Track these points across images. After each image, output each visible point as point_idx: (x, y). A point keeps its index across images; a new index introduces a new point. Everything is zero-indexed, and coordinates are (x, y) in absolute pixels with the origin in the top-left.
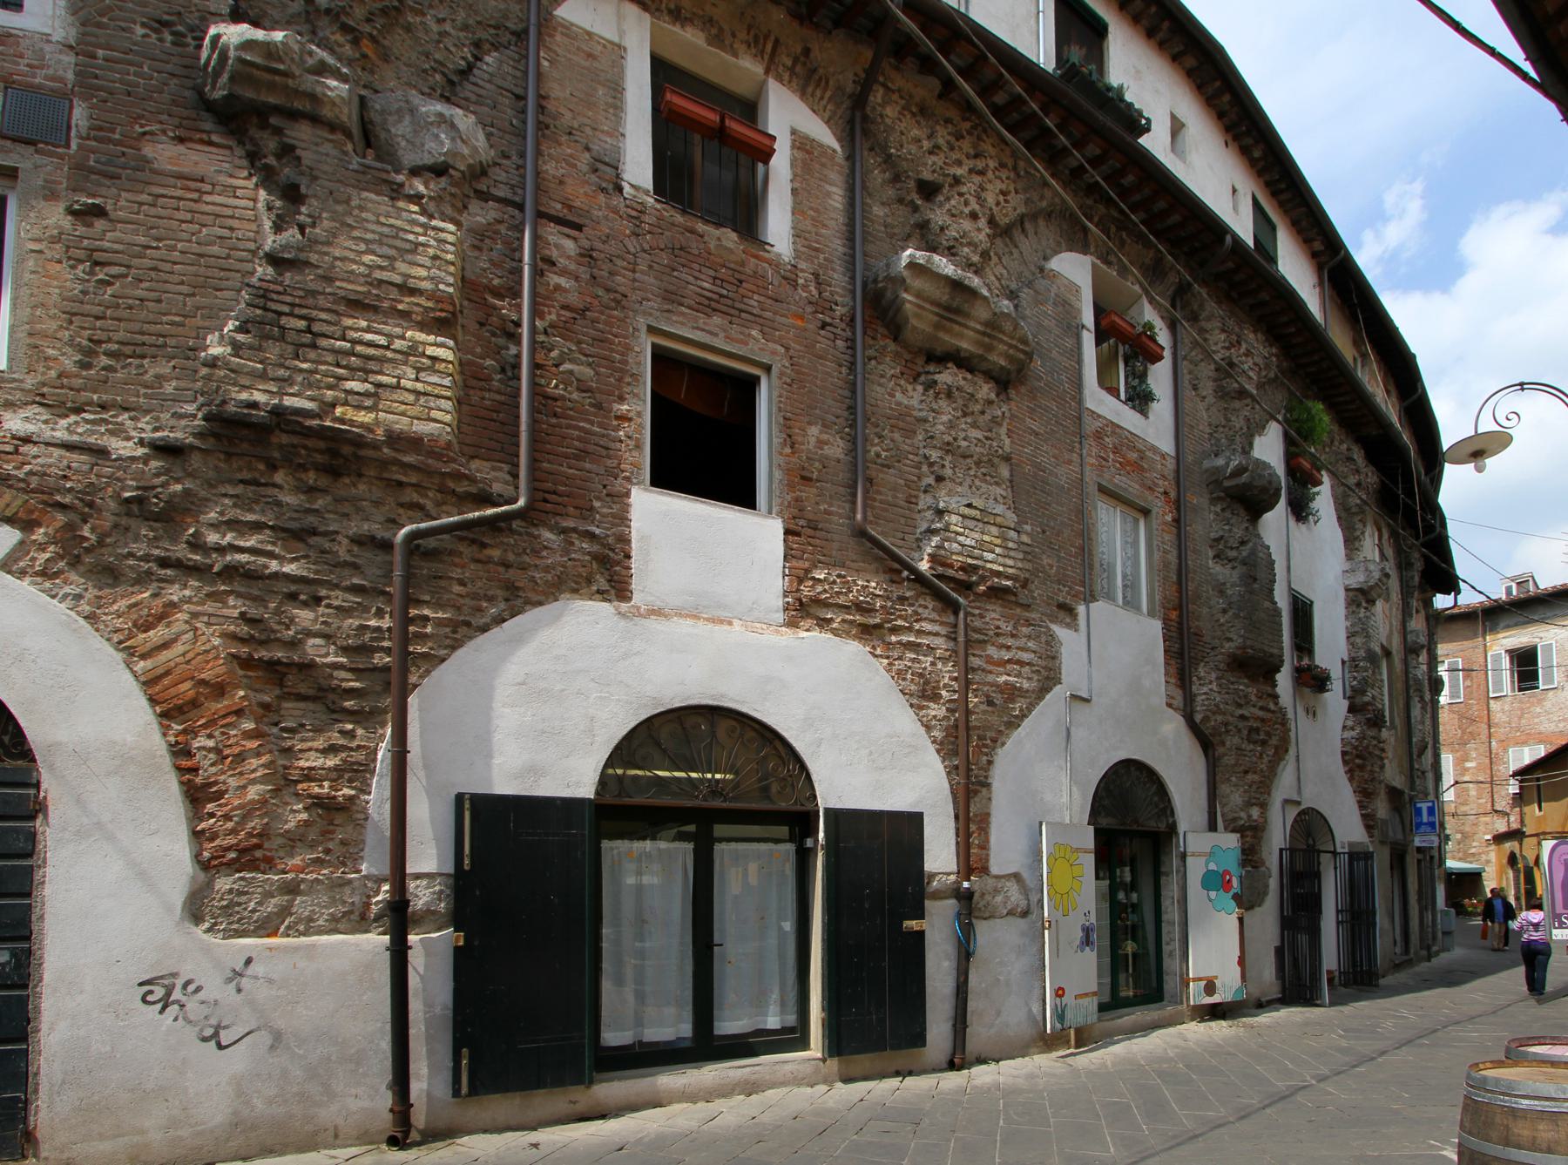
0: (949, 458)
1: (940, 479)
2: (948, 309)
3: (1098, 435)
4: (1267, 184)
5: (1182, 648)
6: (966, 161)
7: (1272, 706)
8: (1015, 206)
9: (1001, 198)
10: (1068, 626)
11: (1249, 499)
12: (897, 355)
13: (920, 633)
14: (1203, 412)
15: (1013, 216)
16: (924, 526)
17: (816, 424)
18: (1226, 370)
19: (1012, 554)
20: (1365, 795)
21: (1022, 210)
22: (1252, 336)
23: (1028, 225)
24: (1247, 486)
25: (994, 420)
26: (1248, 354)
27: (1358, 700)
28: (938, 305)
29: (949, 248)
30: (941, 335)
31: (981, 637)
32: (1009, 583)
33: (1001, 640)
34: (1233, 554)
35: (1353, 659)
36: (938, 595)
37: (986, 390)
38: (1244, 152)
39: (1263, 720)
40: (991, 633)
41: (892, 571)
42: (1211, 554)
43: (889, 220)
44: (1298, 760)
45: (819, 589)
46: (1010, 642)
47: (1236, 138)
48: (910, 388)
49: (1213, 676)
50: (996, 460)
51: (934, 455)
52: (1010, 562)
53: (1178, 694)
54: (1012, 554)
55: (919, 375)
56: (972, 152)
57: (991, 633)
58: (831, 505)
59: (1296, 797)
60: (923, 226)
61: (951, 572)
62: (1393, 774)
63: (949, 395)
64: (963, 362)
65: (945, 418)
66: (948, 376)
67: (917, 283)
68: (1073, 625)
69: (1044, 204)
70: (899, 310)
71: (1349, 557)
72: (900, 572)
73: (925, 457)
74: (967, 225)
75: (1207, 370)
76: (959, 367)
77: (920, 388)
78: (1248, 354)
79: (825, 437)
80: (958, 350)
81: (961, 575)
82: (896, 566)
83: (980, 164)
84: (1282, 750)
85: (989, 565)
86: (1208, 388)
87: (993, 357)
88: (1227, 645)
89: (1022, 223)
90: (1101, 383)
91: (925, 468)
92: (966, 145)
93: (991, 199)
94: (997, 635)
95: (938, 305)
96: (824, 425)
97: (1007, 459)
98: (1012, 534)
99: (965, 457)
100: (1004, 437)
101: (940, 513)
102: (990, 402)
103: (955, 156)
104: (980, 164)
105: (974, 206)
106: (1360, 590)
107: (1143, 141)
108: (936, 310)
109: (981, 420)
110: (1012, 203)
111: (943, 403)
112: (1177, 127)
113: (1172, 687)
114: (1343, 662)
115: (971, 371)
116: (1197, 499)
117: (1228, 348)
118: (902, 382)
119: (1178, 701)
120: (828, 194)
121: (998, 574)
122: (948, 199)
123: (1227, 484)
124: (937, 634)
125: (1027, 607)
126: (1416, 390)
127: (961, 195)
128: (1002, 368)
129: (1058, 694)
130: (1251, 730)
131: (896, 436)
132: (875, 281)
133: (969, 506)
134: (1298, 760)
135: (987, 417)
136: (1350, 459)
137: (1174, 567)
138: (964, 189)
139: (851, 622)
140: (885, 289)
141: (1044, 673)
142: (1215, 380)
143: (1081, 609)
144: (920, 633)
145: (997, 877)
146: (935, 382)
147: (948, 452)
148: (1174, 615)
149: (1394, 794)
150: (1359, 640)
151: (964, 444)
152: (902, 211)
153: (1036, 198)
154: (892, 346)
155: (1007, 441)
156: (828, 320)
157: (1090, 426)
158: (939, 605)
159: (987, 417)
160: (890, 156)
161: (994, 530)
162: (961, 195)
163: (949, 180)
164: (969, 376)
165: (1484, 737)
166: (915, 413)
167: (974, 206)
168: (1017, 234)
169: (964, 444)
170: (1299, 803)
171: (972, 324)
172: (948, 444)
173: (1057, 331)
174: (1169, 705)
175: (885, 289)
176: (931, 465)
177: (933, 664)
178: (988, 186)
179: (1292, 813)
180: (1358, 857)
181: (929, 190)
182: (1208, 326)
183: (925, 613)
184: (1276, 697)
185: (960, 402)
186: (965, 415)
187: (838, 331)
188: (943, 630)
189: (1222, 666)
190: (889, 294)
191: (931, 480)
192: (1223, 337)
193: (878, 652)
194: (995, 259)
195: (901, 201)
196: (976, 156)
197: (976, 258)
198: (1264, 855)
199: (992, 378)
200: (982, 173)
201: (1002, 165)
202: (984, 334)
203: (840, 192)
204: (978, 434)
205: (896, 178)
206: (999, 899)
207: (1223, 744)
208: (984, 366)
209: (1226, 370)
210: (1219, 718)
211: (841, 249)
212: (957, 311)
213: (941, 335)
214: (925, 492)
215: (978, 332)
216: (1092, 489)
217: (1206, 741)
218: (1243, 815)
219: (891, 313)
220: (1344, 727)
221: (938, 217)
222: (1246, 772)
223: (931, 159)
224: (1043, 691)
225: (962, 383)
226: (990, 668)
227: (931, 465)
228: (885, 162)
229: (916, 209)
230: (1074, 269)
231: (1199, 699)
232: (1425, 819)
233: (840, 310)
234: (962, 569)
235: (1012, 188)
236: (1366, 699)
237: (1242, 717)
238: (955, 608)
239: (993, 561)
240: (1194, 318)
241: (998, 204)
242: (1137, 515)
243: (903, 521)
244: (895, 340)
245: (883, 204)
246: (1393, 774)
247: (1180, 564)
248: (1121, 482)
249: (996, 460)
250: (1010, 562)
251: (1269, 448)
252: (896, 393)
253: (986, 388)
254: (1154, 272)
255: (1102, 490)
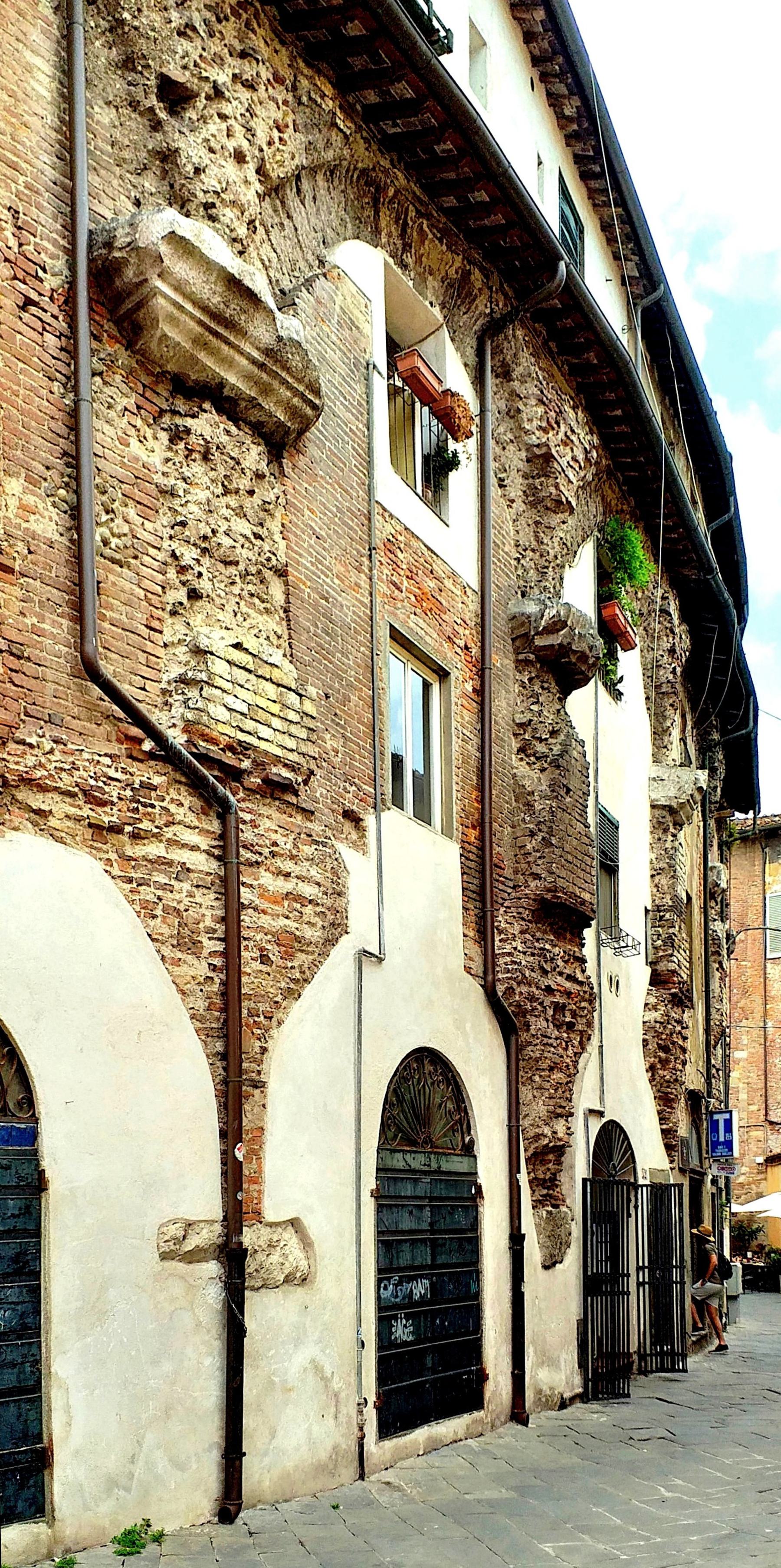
0: (206, 561)
1: (194, 595)
2: (216, 316)
3: (391, 545)
4: (578, 159)
5: (482, 886)
6: (229, 60)
7: (580, 976)
8: (290, 155)
9: (276, 134)
10: (354, 845)
11: (561, 666)
12: (130, 373)
13: (172, 843)
14: (510, 522)
15: (290, 166)
16: (175, 671)
17: (17, 475)
18: (541, 462)
19: (294, 729)
20: (665, 1100)
21: (302, 159)
22: (571, 414)
23: (306, 185)
24: (564, 649)
25: (265, 506)
26: (567, 442)
27: (662, 967)
28: (205, 309)
29: (208, 206)
30: (202, 356)
31: (254, 858)
32: (286, 773)
33: (279, 862)
34: (541, 748)
35: (658, 908)
36: (197, 785)
37: (254, 456)
38: (554, 101)
39: (568, 994)
40: (266, 851)
41: (129, 739)
42: (515, 745)
43: (117, 134)
44: (601, 1053)
45: (31, 761)
46: (287, 866)
47: (544, 77)
48: (149, 433)
49: (516, 929)
50: (268, 574)
51: (189, 555)
52: (291, 743)
53: (475, 951)
54: (294, 729)
55: (162, 412)
56: (239, 47)
57: (266, 851)
58: (42, 620)
59: (597, 1107)
60: (167, 157)
61: (214, 751)
62: (693, 1079)
63: (206, 457)
64: (229, 406)
65: (202, 495)
66: (207, 425)
67: (181, 268)
68: (360, 845)
69: (330, 155)
70: (141, 304)
71: (656, 761)
72: (140, 741)
73: (174, 555)
74: (231, 169)
75: (516, 458)
76: (220, 411)
77: (164, 436)
78: (567, 442)
79: (30, 500)
80: (222, 384)
81: (229, 758)
82: (135, 731)
83: (249, 70)
84: (585, 1039)
85: (263, 745)
86: (516, 486)
87: (268, 404)
88: (533, 884)
89: (298, 178)
90: (394, 461)
91: (172, 573)
92: (230, 29)
93: (262, 138)
94: (273, 855)
95: (205, 309)
96: (28, 479)
97: (282, 573)
98: (293, 698)
99: (227, 563)
100: (277, 537)
101: (199, 652)
102: (260, 476)
103: (215, 46)
104: (249, 70)
105: (240, 140)
106: (671, 810)
107: (444, 59)
108: (198, 314)
109: (252, 504)
110: (290, 147)
111: (197, 469)
112: (478, 44)
113: (470, 943)
114: (647, 911)
115: (235, 419)
116: (501, 660)
117: (545, 431)
118: (139, 423)
119: (477, 966)
120: (29, 69)
121: (277, 760)
122: (203, 119)
123: (539, 642)
124: (194, 848)
125: (308, 814)
126: (728, 510)
127: (223, 117)
128: (280, 424)
129: (344, 952)
130: (559, 1008)
131: (131, 512)
132: (109, 245)
133: (238, 646)
134: (601, 1053)
135: (256, 500)
136: (665, 612)
137: (473, 762)
138: (227, 109)
139: (78, 820)
140: (125, 262)
141: (330, 917)
142: (525, 477)
143: (369, 820)
144: (172, 843)
145: (270, 1225)
146: (188, 431)
147: (205, 551)
148: (473, 834)
149: (694, 1099)
150: (664, 881)
151: (227, 542)
152: (136, 123)
153: (320, 145)
154: (123, 357)
155: (282, 544)
156: (34, 296)
157: (383, 530)
158: (198, 804)
159: (256, 500)
160: (122, 22)
161: (271, 690)
162: (223, 117)
163: (207, 88)
164: (234, 430)
165: (758, 1015)
166: (158, 479)
167: (240, 140)
168: (290, 194)
169: (227, 542)
170: (601, 1114)
171: (248, 348)
172: (205, 538)
173: (343, 369)
174: (468, 970)
175: (125, 262)
176: (183, 570)
177: (191, 895)
178: (258, 109)
179: (595, 1126)
180: (660, 1193)
181: (176, 97)
182: (522, 390)
183: (180, 813)
184: (582, 961)
185: (222, 471)
186: (226, 492)
187: (47, 317)
188: (204, 843)
189: (526, 914)
190: (130, 273)
191: (181, 595)
192: (540, 410)
193: (116, 871)
194: (261, 230)
195: (134, 105)
196: (243, 55)
197: (242, 231)
198: (565, 1189)
199: (262, 435)
200: (250, 86)
201: (278, 79)
202: (262, 366)
203: (48, 69)
204: (242, 527)
205: (128, 63)
206: (275, 1258)
207: (527, 1026)
208: (254, 415)
209: (541, 462)
210: (524, 989)
211: (49, 171)
212: (230, 324)
213: (202, 356)
214: (174, 613)
215: (254, 362)
216: (383, 633)
217: (509, 1022)
218: (547, 1130)
219: (129, 305)
220: (646, 1005)
221: (191, 149)
222: (551, 1069)
223: (183, 45)
224: (331, 942)
225: (225, 439)
226: (264, 905)
227: (183, 570)
228: (111, 30)
229: (156, 126)
230: (364, 265)
231: (501, 961)
232: (722, 1139)
233: (51, 282)
234: (230, 748)
235: (289, 120)
236: (673, 966)
237: (549, 990)
238: (223, 811)
239: (271, 740)
240: (505, 373)
241: (270, 143)
242: (432, 678)
243: (142, 657)
244: (129, 346)
245: (108, 103)
246: (693, 1079)
247: (483, 758)
248: (417, 627)
249: (268, 574)
250: (291, 743)
251: (579, 588)
252: (125, 438)
253: (255, 450)
254: (457, 294)
255: (396, 635)
